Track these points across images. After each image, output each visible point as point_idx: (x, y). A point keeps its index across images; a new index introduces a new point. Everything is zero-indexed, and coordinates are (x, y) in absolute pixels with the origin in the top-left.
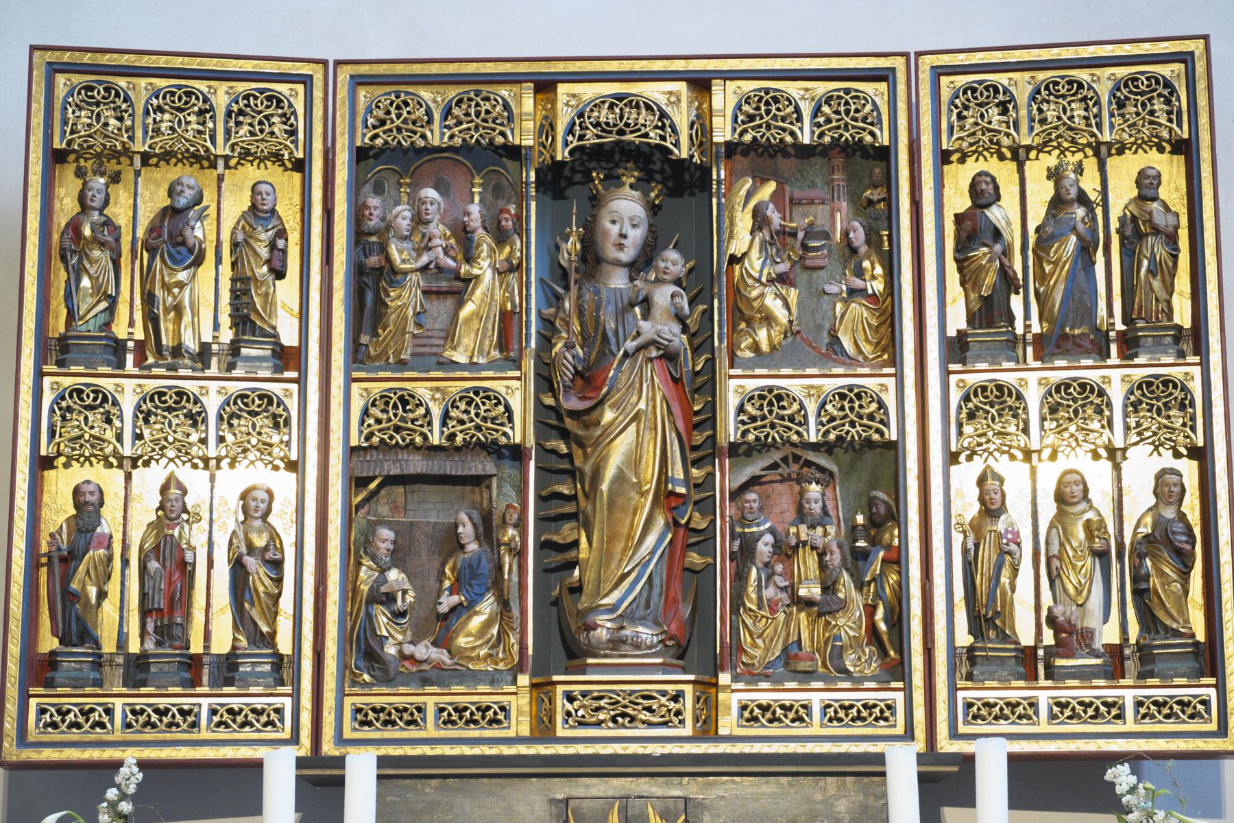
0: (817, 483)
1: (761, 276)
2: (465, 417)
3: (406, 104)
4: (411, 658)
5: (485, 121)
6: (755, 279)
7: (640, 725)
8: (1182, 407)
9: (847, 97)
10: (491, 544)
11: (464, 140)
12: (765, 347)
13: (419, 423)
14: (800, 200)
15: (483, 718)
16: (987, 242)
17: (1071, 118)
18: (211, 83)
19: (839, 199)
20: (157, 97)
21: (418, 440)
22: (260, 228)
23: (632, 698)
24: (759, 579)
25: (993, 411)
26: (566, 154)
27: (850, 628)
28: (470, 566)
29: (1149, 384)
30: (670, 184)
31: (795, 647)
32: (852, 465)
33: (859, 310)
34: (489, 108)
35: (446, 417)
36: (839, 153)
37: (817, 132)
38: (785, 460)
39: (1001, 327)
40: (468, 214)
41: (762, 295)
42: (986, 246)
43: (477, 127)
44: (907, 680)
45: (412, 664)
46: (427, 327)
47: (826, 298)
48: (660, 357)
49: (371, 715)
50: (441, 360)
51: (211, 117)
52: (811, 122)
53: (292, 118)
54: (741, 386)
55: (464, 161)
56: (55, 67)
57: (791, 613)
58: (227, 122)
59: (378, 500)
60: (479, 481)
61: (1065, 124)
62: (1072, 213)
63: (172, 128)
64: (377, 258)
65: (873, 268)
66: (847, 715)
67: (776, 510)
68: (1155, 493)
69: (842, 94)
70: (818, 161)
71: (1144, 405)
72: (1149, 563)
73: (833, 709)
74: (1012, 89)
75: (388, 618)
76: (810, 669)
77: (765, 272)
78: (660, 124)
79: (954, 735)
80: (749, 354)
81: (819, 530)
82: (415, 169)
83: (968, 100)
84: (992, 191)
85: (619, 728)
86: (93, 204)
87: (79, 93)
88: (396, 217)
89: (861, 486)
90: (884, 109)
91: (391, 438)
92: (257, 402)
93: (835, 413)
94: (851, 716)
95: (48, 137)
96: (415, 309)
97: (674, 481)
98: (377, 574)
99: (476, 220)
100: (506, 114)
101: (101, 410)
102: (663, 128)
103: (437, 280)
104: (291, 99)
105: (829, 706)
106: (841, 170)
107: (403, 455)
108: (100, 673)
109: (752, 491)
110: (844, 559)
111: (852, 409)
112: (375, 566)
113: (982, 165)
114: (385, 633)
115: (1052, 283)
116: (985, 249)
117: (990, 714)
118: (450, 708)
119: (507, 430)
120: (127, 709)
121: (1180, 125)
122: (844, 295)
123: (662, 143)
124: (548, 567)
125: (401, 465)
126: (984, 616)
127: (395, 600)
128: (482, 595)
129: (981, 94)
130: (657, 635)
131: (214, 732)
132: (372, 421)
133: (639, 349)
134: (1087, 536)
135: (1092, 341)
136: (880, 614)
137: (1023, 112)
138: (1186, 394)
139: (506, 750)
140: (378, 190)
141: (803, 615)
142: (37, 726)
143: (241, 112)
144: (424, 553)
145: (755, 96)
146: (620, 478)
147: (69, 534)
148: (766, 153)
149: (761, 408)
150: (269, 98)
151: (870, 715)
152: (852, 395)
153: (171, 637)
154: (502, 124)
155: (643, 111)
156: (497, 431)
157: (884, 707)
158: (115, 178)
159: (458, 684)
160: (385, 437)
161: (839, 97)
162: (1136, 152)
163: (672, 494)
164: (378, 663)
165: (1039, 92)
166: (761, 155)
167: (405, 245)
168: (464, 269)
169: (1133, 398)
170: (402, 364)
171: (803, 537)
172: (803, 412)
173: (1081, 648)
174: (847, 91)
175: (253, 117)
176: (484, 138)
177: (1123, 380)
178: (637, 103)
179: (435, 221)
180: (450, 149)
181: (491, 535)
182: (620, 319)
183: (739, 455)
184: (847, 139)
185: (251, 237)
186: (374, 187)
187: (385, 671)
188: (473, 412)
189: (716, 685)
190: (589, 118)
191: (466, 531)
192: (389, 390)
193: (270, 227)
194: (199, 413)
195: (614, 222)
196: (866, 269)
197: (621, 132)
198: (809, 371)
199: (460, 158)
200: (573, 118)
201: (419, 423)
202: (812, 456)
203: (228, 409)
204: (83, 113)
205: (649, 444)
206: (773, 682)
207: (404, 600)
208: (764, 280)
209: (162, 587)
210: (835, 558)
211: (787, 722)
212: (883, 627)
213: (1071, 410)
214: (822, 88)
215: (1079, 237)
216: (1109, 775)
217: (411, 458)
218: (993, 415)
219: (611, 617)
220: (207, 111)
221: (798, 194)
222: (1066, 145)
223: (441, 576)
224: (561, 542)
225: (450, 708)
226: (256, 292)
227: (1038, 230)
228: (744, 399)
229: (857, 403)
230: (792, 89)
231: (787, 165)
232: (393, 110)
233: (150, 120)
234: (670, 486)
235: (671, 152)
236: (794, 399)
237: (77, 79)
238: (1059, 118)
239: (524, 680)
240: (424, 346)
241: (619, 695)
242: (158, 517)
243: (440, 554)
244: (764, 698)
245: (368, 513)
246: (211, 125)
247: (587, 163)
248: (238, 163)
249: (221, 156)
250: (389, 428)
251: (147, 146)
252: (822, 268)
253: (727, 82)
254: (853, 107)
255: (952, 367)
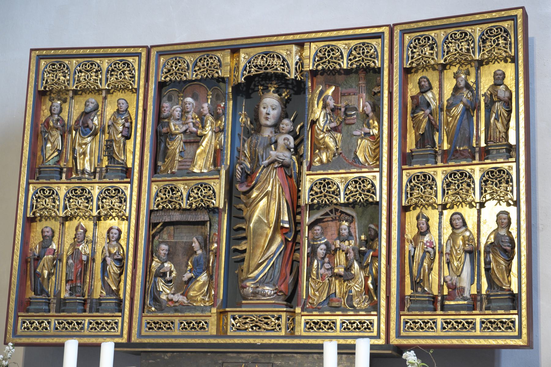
0: (346, 221)
1: (323, 129)
2: (196, 196)
3: (179, 62)
4: (171, 300)
5: (210, 67)
6: (321, 131)
7: (263, 330)
8: (507, 182)
9: (364, 47)
10: (206, 251)
11: (202, 76)
12: (325, 160)
13: (178, 199)
14: (345, 94)
15: (198, 327)
16: (423, 109)
17: (461, 49)
18: (101, 59)
19: (362, 92)
20: (80, 67)
21: (178, 206)
22: (119, 119)
23: (260, 318)
24: (318, 265)
25: (422, 187)
26: (243, 79)
27: (357, 287)
28: (197, 260)
29: (492, 172)
30: (295, 89)
31: (333, 295)
32: (363, 213)
33: (365, 143)
34: (212, 62)
35: (189, 196)
36: (362, 71)
37: (350, 63)
38: (331, 211)
39: (427, 148)
40: (203, 108)
41: (324, 137)
42: (423, 110)
43: (207, 71)
44: (378, 311)
45: (172, 303)
46: (185, 157)
47: (354, 137)
48: (281, 167)
49: (153, 325)
50: (188, 171)
51: (101, 73)
52: (347, 59)
53: (133, 72)
54: (312, 179)
55: (203, 85)
56: (40, 57)
57: (332, 280)
58: (107, 74)
59: (163, 232)
60: (203, 223)
61: (458, 52)
62: (462, 93)
63: (85, 79)
64: (166, 128)
65: (374, 123)
66: (352, 327)
67: (329, 234)
68: (497, 223)
69: (361, 45)
70: (354, 75)
71: (489, 182)
72: (491, 256)
73: (366, 324)
74: (436, 38)
75: (163, 284)
76: (337, 306)
77: (326, 127)
78: (282, 64)
79: (519, 336)
80: (318, 164)
81: (347, 242)
82: (184, 89)
83: (416, 44)
84: (427, 85)
85: (254, 331)
86: (54, 112)
87: (49, 67)
88: (173, 111)
89: (367, 222)
90: (379, 50)
91: (167, 206)
92: (114, 192)
93: (352, 189)
94: (354, 327)
95: (36, 86)
96: (179, 150)
97: (284, 222)
98: (160, 264)
99: (206, 110)
100: (219, 64)
101: (52, 197)
102: (284, 66)
103: (189, 137)
104: (133, 63)
105: (344, 323)
106: (363, 79)
107: (172, 213)
108: (49, 306)
109: (319, 226)
110: (355, 255)
111: (360, 187)
112: (159, 261)
113: (425, 74)
114: (161, 290)
115: (451, 127)
116: (423, 112)
117: (415, 327)
118: (357, 322)
119: (213, 201)
120: (443, 321)
121: (511, 51)
122: (363, 136)
123: (283, 72)
124: (237, 260)
125: (170, 217)
126: (415, 281)
127: (166, 276)
128: (201, 273)
129: (422, 41)
130: (273, 290)
131: (90, 331)
132: (159, 199)
133: (269, 164)
134: (463, 244)
135: (469, 153)
136: (369, 282)
137: (440, 48)
138: (509, 176)
139: (205, 341)
140: (170, 99)
141: (337, 282)
142: (21, 329)
143: (113, 70)
144: (180, 255)
145: (323, 49)
146: (259, 221)
147: (39, 249)
148: (331, 74)
149: (320, 188)
150: (124, 64)
151: (362, 326)
152: (360, 181)
153: (76, 292)
154: (217, 68)
155: (276, 59)
156: (209, 201)
157: (368, 323)
158: (65, 101)
159: (189, 312)
160: (165, 205)
161: (360, 47)
162: (494, 63)
163: (283, 228)
164: (158, 303)
165: (447, 39)
166: (329, 74)
167: (178, 122)
168: (199, 132)
169: (484, 179)
170: (173, 174)
171: (338, 246)
172: (338, 190)
173: (459, 296)
174: (364, 44)
175: (118, 72)
176: (210, 75)
177: (480, 170)
178: (273, 56)
179: (192, 111)
180: (196, 80)
181: (207, 248)
182: (265, 151)
183: (314, 209)
184: (363, 65)
185: (115, 122)
186: (168, 98)
187: (161, 306)
188: (199, 194)
189: (294, 312)
190: (253, 63)
191: (196, 245)
192: (167, 185)
193: (123, 118)
194: (90, 197)
195: (264, 108)
196: (371, 123)
197: (266, 69)
198: (341, 171)
199: (202, 84)
200: (246, 64)
201: (178, 199)
202: (344, 209)
203: (101, 195)
204: (50, 75)
205: (273, 205)
206: (342, 311)
207: (170, 275)
208: (325, 130)
209: (73, 271)
210: (351, 255)
211: (326, 329)
212: (371, 286)
213: (456, 185)
214: (353, 43)
215: (465, 105)
216: (404, 355)
217: (175, 214)
218: (421, 189)
219: (253, 282)
220: (99, 71)
221: (344, 91)
222: (462, 61)
223: (187, 265)
224: (240, 249)
225: (347, 322)
226: (116, 146)
227: (448, 101)
228: (158, 190)
229: (362, 184)
230: (341, 45)
231: (340, 78)
232: (174, 65)
233: (76, 76)
234: (281, 224)
235: (287, 76)
236: (335, 184)
237: (48, 61)
238: (456, 50)
239: (214, 310)
240: (183, 165)
241: (254, 317)
242: (74, 241)
243: (187, 255)
244: (316, 319)
245: (159, 238)
246: (100, 76)
247: (261, 82)
248: (114, 91)
249: (104, 89)
250: (166, 202)
251: (74, 86)
252: (353, 124)
253: (312, 44)
254: (366, 51)
255: (404, 167)
